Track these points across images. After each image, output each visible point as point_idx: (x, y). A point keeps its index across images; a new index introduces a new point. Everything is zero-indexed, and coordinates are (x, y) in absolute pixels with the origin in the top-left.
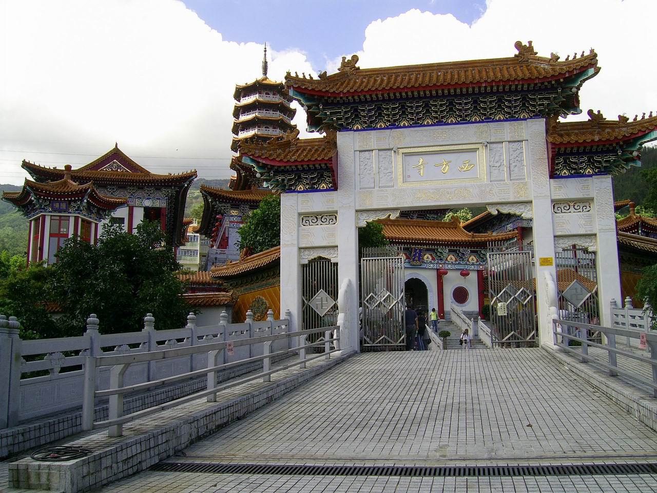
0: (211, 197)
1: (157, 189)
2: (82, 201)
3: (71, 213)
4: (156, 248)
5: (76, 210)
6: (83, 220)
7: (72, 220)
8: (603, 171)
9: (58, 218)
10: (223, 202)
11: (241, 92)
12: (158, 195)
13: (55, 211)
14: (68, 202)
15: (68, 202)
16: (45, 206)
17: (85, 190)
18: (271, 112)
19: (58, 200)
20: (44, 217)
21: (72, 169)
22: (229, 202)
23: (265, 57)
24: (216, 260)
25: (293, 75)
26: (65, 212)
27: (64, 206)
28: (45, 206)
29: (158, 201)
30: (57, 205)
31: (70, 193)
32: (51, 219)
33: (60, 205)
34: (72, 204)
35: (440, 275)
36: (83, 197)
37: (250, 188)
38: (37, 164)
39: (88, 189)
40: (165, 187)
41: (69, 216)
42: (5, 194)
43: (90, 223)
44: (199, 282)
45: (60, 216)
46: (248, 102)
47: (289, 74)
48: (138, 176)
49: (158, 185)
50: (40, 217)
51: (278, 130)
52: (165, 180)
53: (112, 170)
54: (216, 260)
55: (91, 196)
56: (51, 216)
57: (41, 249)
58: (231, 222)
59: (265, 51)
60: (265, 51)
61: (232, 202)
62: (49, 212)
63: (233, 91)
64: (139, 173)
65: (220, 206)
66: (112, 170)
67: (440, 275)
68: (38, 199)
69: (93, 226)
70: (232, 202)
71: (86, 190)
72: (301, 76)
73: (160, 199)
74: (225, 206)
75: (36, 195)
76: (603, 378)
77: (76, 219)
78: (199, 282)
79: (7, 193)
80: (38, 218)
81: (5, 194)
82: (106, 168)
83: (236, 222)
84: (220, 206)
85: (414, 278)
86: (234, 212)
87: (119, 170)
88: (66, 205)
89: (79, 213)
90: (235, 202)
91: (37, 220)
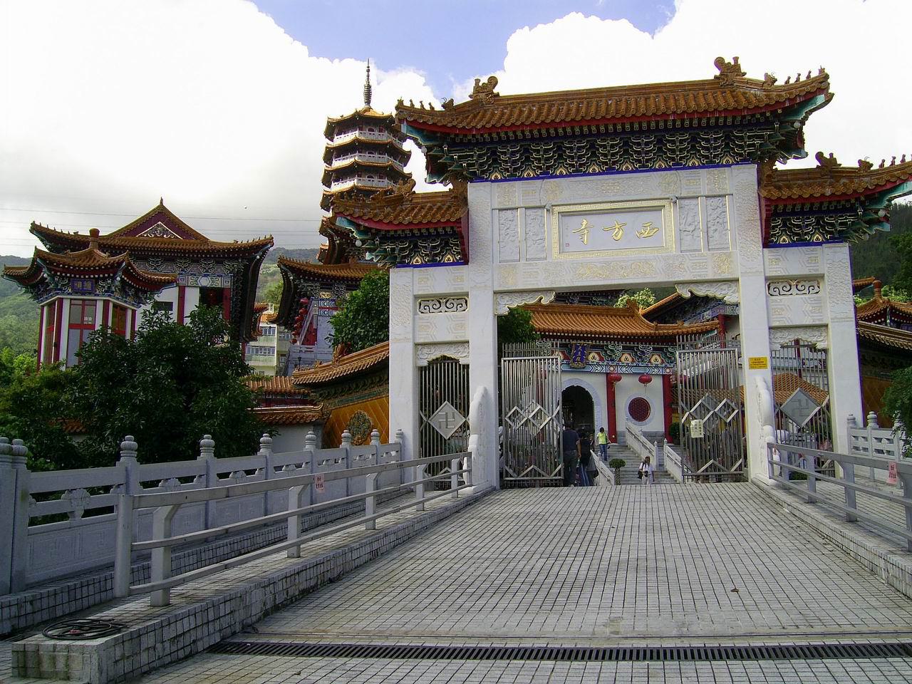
0: (293, 273)
1: (218, 263)
2: (114, 279)
3: (98, 295)
4: (217, 344)
5: (106, 292)
6: (115, 306)
7: (100, 305)
9: (81, 302)
10: (309, 280)
11: (335, 128)
12: (219, 270)
13: (77, 293)
14: (94, 280)
15: (94, 280)
16: (63, 285)
17: (117, 263)
18: (377, 155)
19: (80, 277)
20: (61, 301)
21: (100, 235)
22: (318, 281)
23: (368, 79)
24: (300, 361)
25: (407, 103)
26: (90, 293)
28: (63, 285)
29: (220, 279)
30: (79, 285)
31: (97, 268)
32: (71, 305)
33: (83, 284)
35: (611, 381)
36: (115, 274)
37: (347, 261)
38: (51, 228)
39: (122, 262)
40: (230, 259)
41: (96, 300)
42: (6, 269)
43: (125, 309)
45: (84, 300)
46: (344, 141)
47: (401, 102)
48: (191, 245)
50: (55, 301)
52: (229, 250)
53: (156, 236)
54: (300, 361)
56: (71, 299)
57: (57, 346)
58: (320, 308)
59: (368, 71)
60: (368, 71)
62: (69, 294)
63: (324, 127)
64: (194, 240)
65: (305, 285)
66: (156, 236)
67: (611, 381)
68: (53, 277)
69: (129, 313)
70: (322, 280)
71: (120, 264)
72: (418, 106)
73: (221, 276)
74: (312, 286)
75: (50, 270)
77: (106, 303)
79: (9, 268)
80: (53, 303)
81: (6, 269)
82: (147, 233)
83: (327, 308)
84: (305, 285)
85: (575, 386)
86: (325, 295)
87: (165, 236)
88: (92, 284)
89: (110, 296)
90: (327, 281)
91: (51, 305)
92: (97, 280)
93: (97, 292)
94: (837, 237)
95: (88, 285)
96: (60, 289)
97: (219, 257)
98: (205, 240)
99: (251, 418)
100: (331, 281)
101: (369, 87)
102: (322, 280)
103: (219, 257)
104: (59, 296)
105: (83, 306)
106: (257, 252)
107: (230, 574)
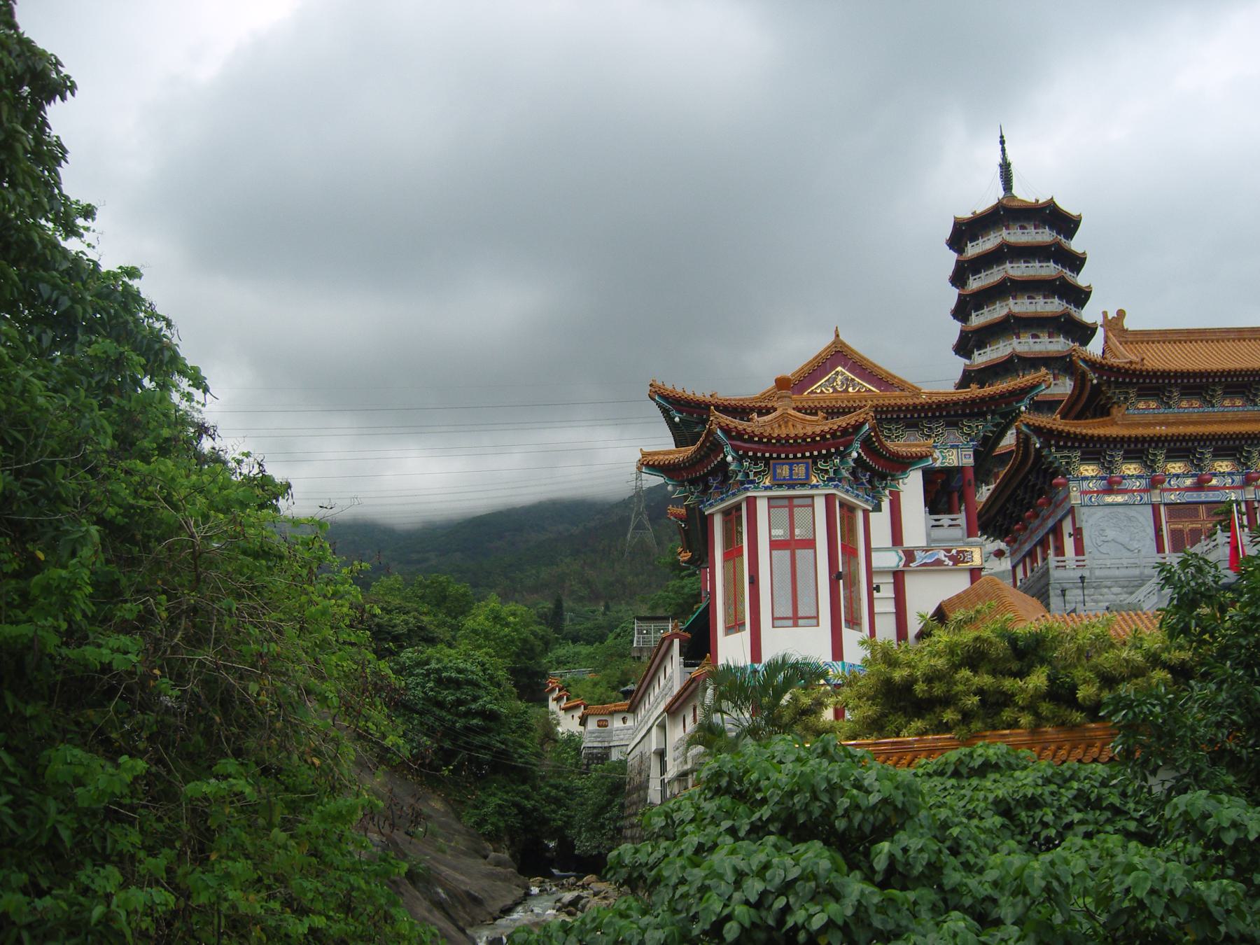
0: (1039, 438)
1: (949, 424)
2: (844, 456)
3: (816, 487)
4: (963, 562)
5: (830, 479)
7: (820, 505)
9: (786, 502)
10: (1065, 447)
11: (963, 232)
12: (952, 437)
13: (780, 486)
14: (810, 461)
15: (810, 461)
16: (756, 474)
17: (853, 426)
18: (1037, 264)
19: (787, 457)
20: (752, 502)
23: (1003, 150)
24: (1083, 582)
26: (803, 485)
29: (955, 451)
30: (784, 471)
32: (769, 507)
33: (791, 470)
34: (821, 465)
36: (848, 445)
37: (1108, 414)
38: (679, 390)
39: (863, 424)
40: (972, 416)
41: (812, 497)
42: (645, 455)
45: (791, 498)
46: (1019, 241)
48: (894, 398)
50: (743, 500)
51: (1056, 300)
52: (1155, 373)
53: (835, 391)
54: (1083, 582)
56: (770, 498)
57: (835, 577)
58: (1084, 493)
59: (1002, 142)
60: (1002, 142)
61: (1087, 446)
62: (766, 488)
63: (948, 231)
64: (897, 393)
65: (1056, 456)
66: (835, 391)
68: (740, 459)
70: (1087, 446)
71: (858, 427)
73: (957, 447)
74: (1069, 457)
75: (736, 449)
77: (829, 499)
79: (649, 454)
80: (738, 507)
81: (645, 455)
82: (822, 389)
83: (1094, 492)
84: (1056, 456)
86: (1089, 470)
87: (850, 389)
88: (807, 469)
89: (836, 486)
90: (1094, 446)
91: (726, 513)
94: (1017, 445)
95: (800, 470)
96: (752, 482)
97: (948, 415)
99: (362, 724)
101: (1002, 137)
103: (948, 415)
104: (749, 494)
107: (453, 933)
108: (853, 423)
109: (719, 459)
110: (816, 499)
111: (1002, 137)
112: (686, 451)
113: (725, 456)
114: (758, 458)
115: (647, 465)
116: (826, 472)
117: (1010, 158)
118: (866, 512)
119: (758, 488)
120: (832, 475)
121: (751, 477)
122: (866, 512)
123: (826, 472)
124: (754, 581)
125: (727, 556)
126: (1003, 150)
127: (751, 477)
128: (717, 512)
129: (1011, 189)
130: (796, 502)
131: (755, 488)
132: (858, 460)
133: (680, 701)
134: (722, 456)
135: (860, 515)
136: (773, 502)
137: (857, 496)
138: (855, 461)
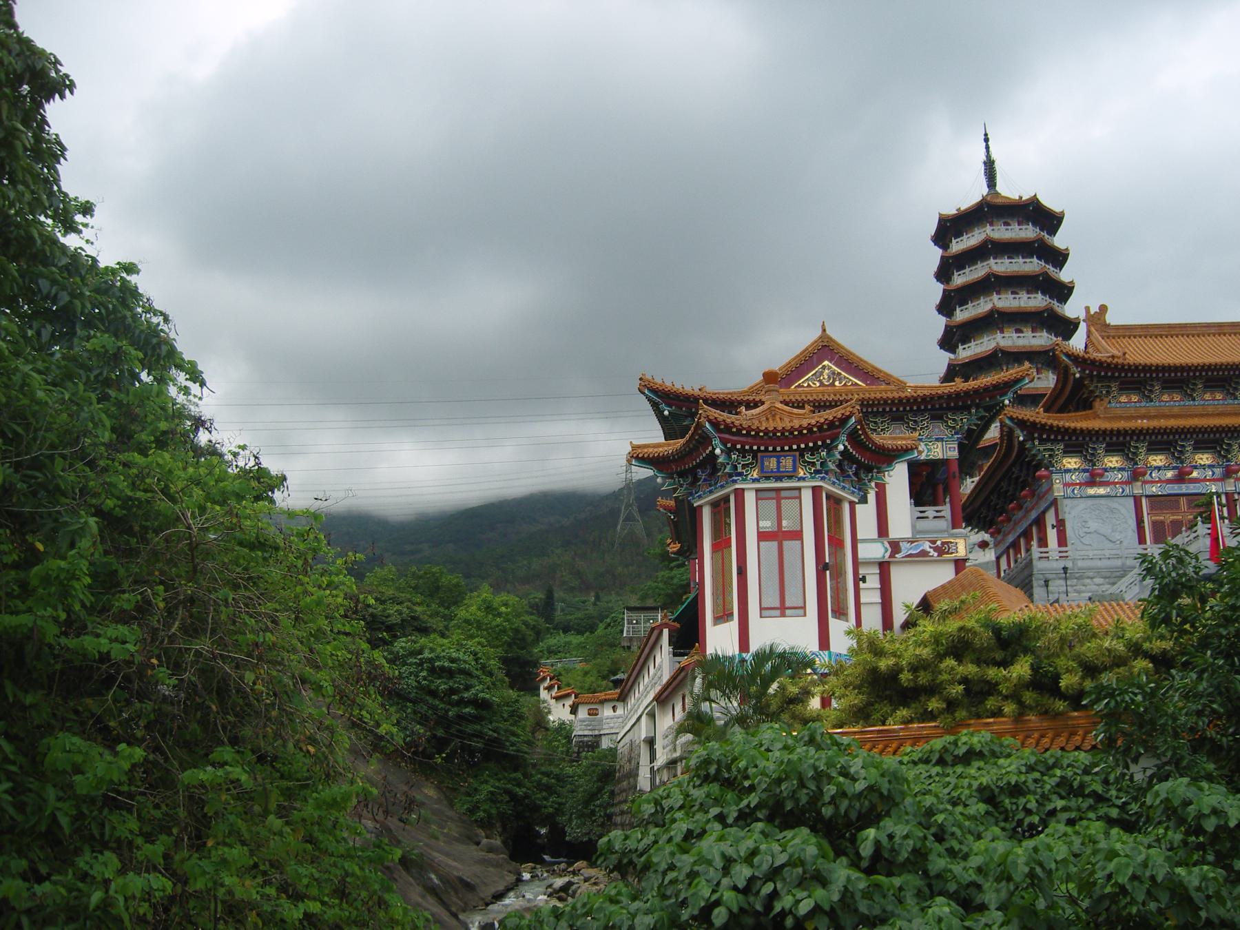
0: (1022, 431)
1: (934, 418)
2: (830, 449)
3: (803, 479)
4: (948, 553)
5: (817, 472)
7: (807, 497)
8: (1001, 438)
9: (773, 494)
10: (1048, 440)
11: (948, 229)
12: (936, 430)
13: (767, 478)
14: (797, 454)
15: (797, 454)
16: (744, 466)
17: (839, 419)
18: (1021, 260)
19: (774, 450)
20: (740, 494)
22: (1062, 440)
23: (987, 148)
24: (1066, 573)
26: (790, 477)
27: (787, 463)
29: (939, 444)
30: (772, 463)
32: (757, 499)
33: (778, 463)
36: (834, 438)
37: (1091, 407)
38: (668, 384)
39: (849, 417)
40: (956, 409)
41: (799, 489)
42: (634, 448)
44: (730, 673)
45: (778, 490)
46: (1003, 237)
48: (879, 392)
49: (933, 408)
50: (731, 492)
52: (1137, 367)
53: (822, 384)
54: (1066, 573)
55: (853, 437)
56: (757, 490)
57: (822, 568)
58: (1067, 485)
59: (986, 140)
60: (986, 140)
62: (754, 481)
63: (933, 228)
64: (883, 387)
65: (1039, 449)
66: (822, 384)
68: (728, 452)
69: (846, 507)
70: (1070, 439)
71: (844, 420)
73: (942, 440)
74: (1052, 450)
75: (724, 442)
76: (450, 866)
77: (816, 491)
78: (730, 673)
79: (639, 447)
80: (726, 499)
81: (634, 448)
82: (809, 383)
83: (1077, 484)
84: (1039, 449)
86: (1072, 462)
87: (837, 383)
88: (794, 461)
89: (823, 479)
90: (1077, 439)
91: (715, 505)
92: (802, 453)
93: (801, 474)
98: (902, 385)
100: (1125, 438)
101: (986, 135)
102: (1070, 439)
104: (737, 486)
105: (779, 500)
106: (1004, 394)
108: (839, 416)
109: (708, 452)
110: (803, 492)
111: (986, 135)
112: (675, 444)
113: (714, 449)
114: (746, 451)
115: (637, 458)
116: (813, 464)
117: (994, 156)
118: (852, 504)
119: (746, 480)
120: (818, 467)
121: (740, 470)
122: (852, 504)
123: (813, 464)
124: (742, 572)
125: (716, 547)
126: (987, 148)
127: (740, 470)
128: (706, 503)
129: (995, 186)
130: (783, 494)
131: (743, 480)
132: (844, 453)
133: (669, 690)
134: (710, 448)
135: (846, 507)
136: (761, 494)
137: (844, 488)
138: (842, 453)
